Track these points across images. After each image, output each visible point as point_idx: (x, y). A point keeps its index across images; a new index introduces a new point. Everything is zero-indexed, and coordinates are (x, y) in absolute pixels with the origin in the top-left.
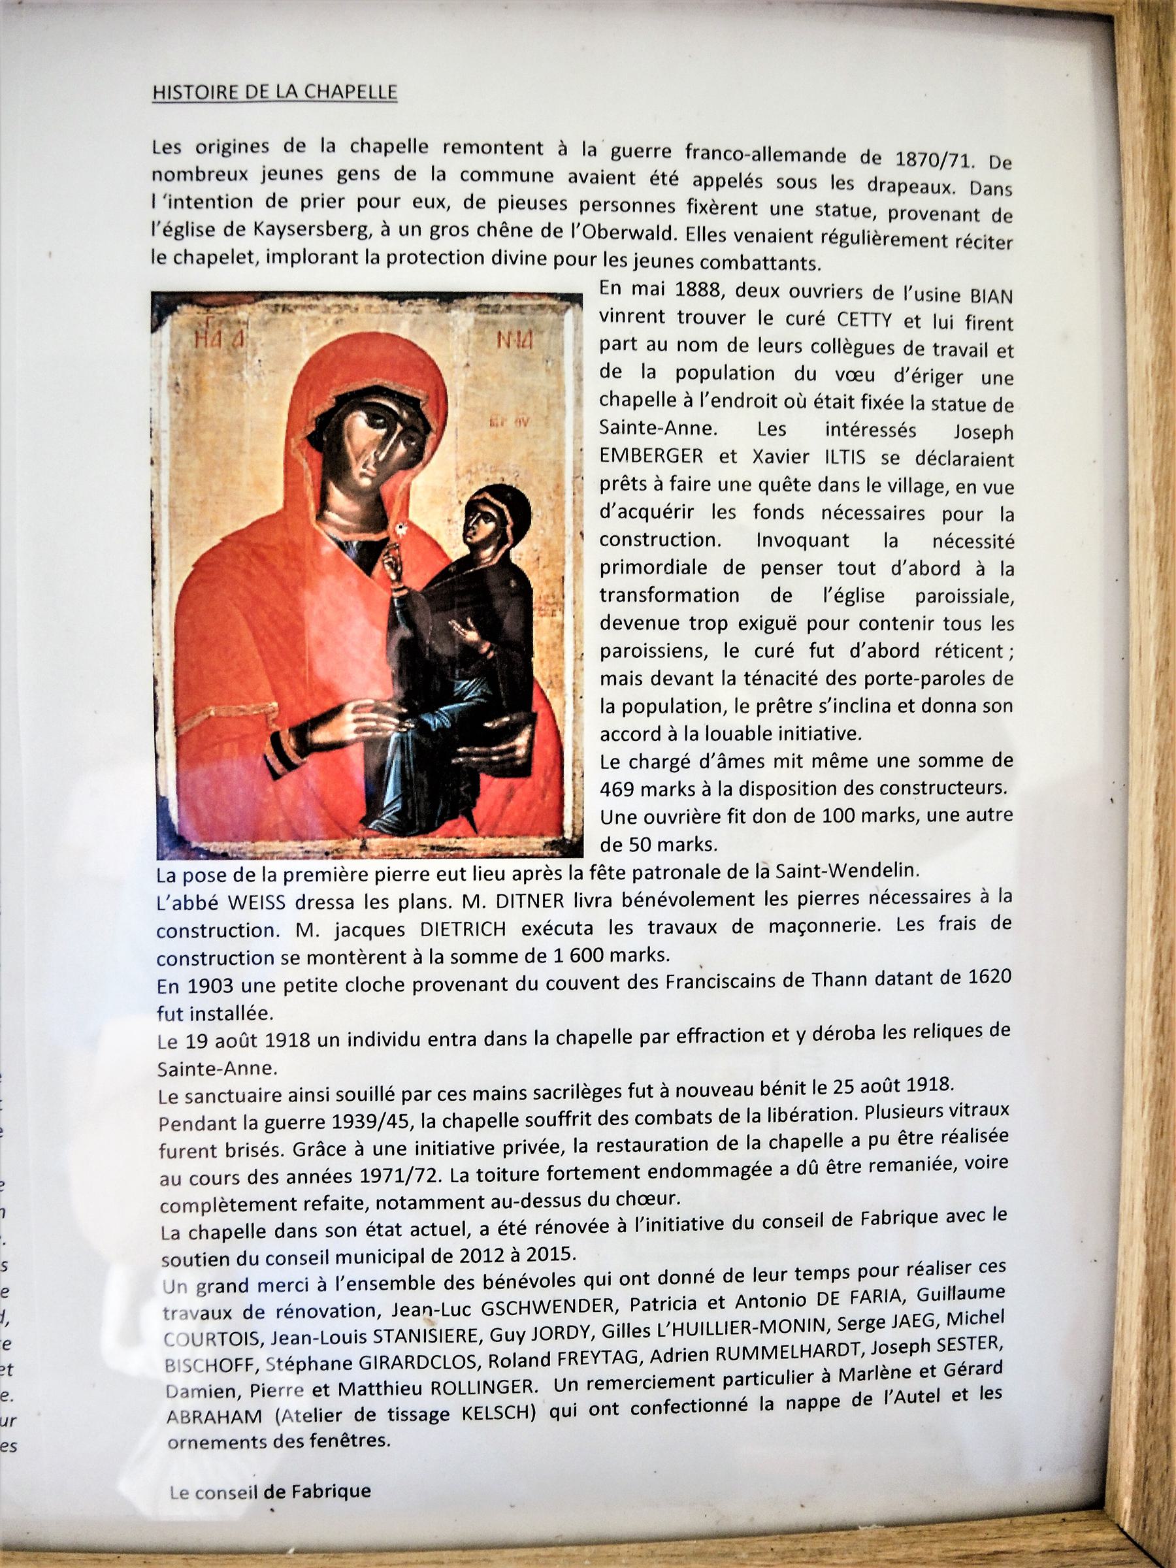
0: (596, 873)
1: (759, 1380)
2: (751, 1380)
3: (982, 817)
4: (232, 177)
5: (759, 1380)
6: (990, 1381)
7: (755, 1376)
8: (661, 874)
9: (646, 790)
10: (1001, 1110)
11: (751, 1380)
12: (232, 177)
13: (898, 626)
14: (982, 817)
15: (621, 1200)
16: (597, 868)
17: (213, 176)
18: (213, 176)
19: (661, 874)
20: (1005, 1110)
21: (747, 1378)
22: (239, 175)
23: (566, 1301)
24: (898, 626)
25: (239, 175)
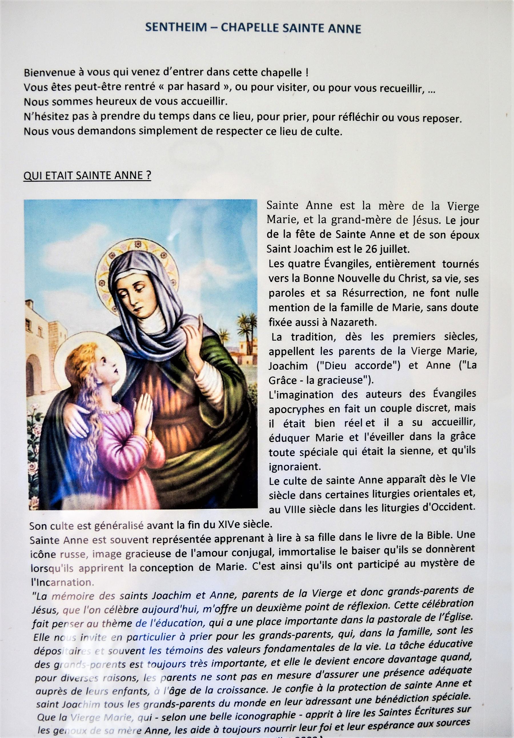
0: (299, 234)
1: (377, 565)
2: (373, 565)
3: (374, 396)
4: (128, 103)
5: (377, 565)
6: (467, 624)
7: (375, 563)
8: (310, 264)
9: (272, 308)
10: (475, 236)
11: (373, 565)
12: (128, 103)
13: (359, 235)
14: (374, 396)
15: (220, 691)
16: (300, 232)
17: (110, 117)
18: (110, 117)
19: (310, 264)
20: (477, 236)
21: (371, 563)
22: (132, 102)
23: (336, 325)
24: (359, 235)
25: (132, 102)
